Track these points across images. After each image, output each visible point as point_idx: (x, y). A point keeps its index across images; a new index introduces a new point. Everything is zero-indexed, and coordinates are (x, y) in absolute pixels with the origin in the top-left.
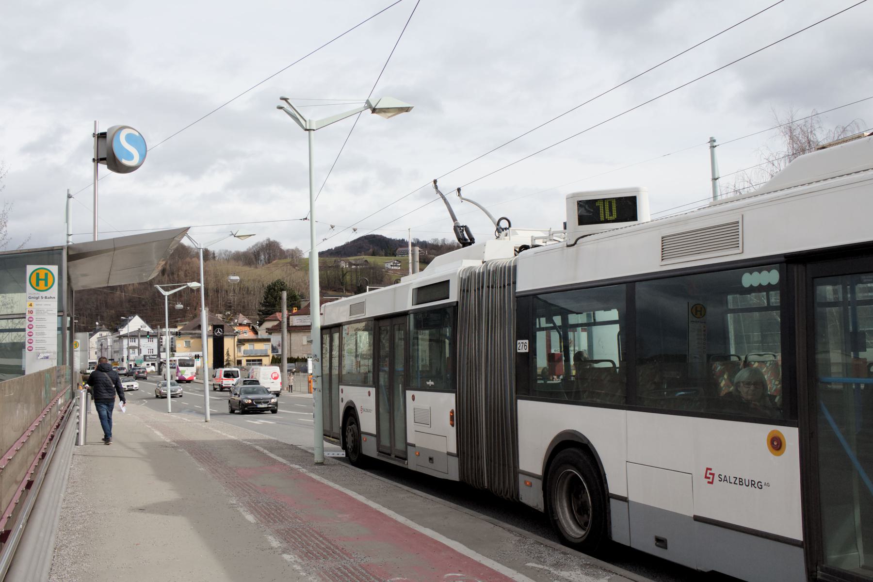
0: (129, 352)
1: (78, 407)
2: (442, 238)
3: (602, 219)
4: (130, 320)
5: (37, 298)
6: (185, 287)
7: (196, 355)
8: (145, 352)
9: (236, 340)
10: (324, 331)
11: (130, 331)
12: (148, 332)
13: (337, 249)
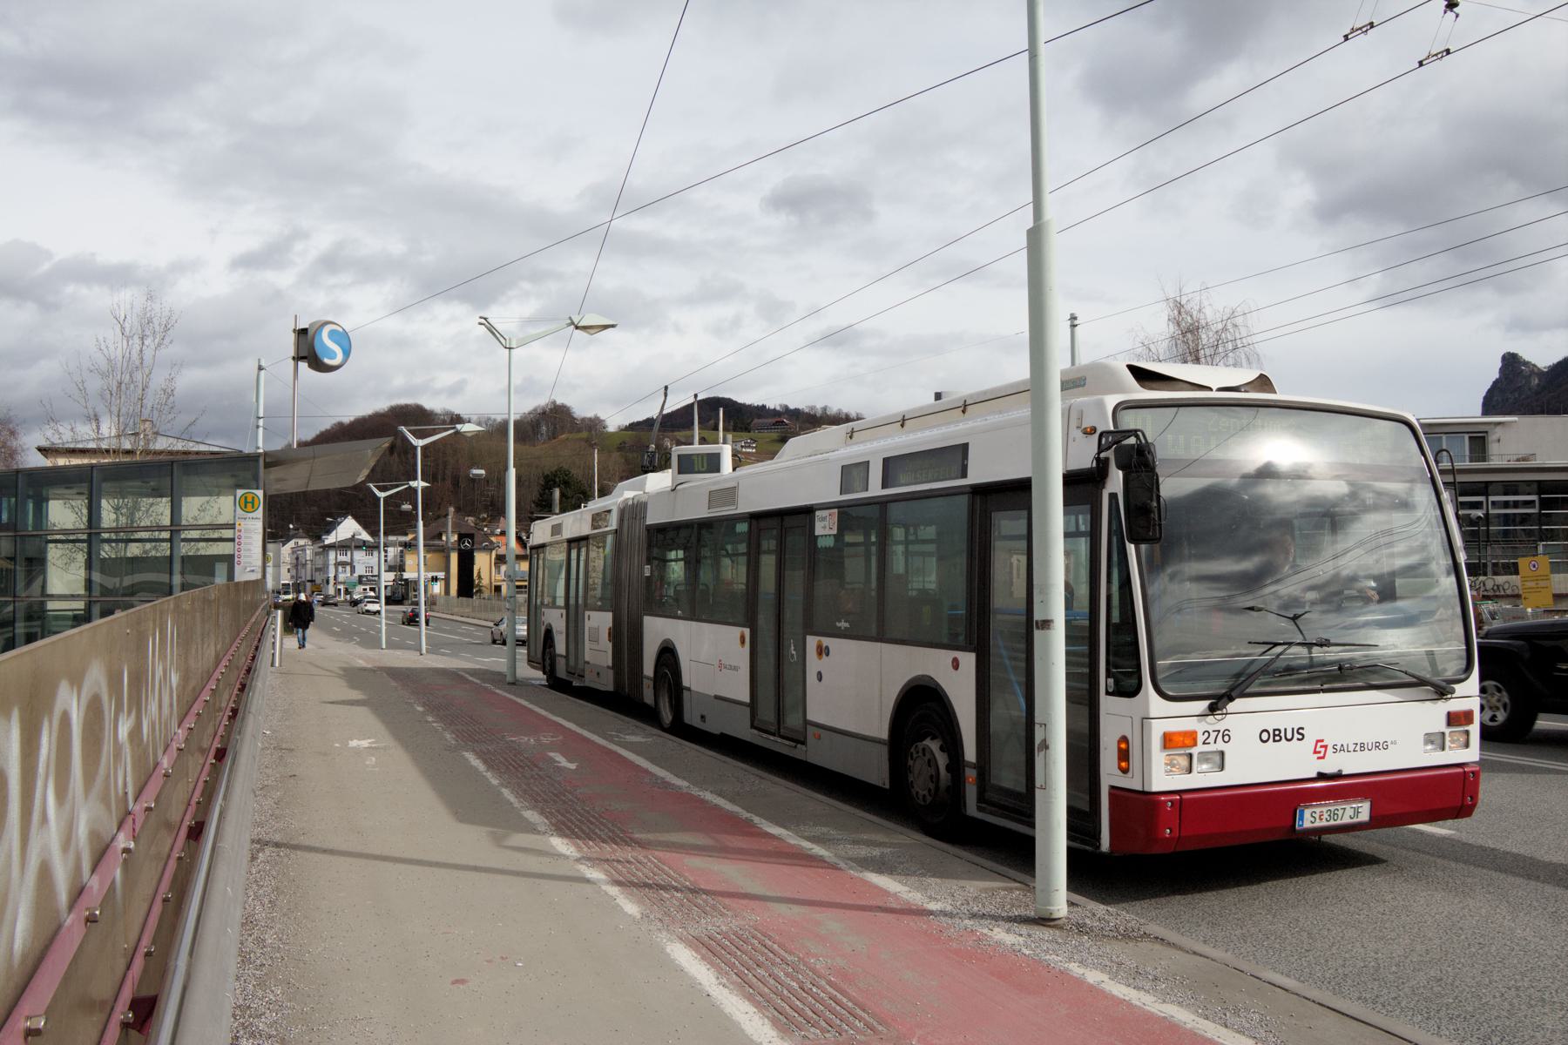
0: (337, 571)
1: (273, 626)
2: (823, 406)
3: (696, 469)
4: (339, 523)
5: (245, 519)
6: (406, 486)
7: (433, 577)
8: (360, 570)
9: (494, 556)
10: (573, 545)
11: (338, 540)
12: (364, 542)
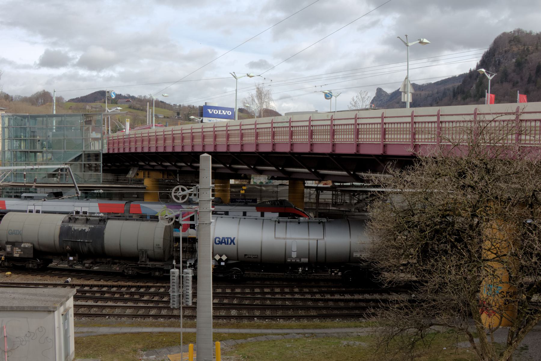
13: (81, 97)
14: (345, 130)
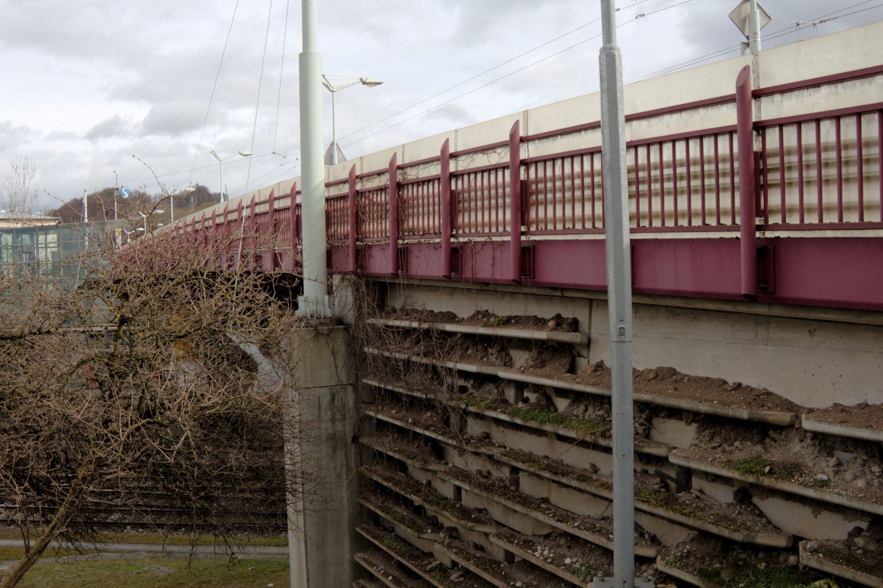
14: (655, 173)
